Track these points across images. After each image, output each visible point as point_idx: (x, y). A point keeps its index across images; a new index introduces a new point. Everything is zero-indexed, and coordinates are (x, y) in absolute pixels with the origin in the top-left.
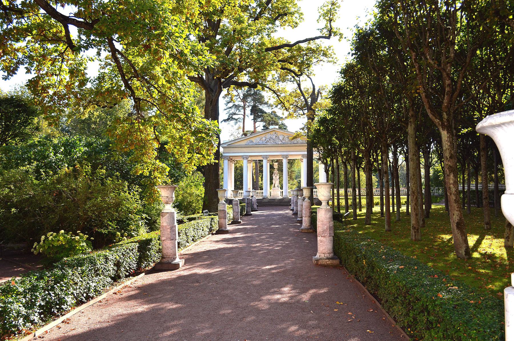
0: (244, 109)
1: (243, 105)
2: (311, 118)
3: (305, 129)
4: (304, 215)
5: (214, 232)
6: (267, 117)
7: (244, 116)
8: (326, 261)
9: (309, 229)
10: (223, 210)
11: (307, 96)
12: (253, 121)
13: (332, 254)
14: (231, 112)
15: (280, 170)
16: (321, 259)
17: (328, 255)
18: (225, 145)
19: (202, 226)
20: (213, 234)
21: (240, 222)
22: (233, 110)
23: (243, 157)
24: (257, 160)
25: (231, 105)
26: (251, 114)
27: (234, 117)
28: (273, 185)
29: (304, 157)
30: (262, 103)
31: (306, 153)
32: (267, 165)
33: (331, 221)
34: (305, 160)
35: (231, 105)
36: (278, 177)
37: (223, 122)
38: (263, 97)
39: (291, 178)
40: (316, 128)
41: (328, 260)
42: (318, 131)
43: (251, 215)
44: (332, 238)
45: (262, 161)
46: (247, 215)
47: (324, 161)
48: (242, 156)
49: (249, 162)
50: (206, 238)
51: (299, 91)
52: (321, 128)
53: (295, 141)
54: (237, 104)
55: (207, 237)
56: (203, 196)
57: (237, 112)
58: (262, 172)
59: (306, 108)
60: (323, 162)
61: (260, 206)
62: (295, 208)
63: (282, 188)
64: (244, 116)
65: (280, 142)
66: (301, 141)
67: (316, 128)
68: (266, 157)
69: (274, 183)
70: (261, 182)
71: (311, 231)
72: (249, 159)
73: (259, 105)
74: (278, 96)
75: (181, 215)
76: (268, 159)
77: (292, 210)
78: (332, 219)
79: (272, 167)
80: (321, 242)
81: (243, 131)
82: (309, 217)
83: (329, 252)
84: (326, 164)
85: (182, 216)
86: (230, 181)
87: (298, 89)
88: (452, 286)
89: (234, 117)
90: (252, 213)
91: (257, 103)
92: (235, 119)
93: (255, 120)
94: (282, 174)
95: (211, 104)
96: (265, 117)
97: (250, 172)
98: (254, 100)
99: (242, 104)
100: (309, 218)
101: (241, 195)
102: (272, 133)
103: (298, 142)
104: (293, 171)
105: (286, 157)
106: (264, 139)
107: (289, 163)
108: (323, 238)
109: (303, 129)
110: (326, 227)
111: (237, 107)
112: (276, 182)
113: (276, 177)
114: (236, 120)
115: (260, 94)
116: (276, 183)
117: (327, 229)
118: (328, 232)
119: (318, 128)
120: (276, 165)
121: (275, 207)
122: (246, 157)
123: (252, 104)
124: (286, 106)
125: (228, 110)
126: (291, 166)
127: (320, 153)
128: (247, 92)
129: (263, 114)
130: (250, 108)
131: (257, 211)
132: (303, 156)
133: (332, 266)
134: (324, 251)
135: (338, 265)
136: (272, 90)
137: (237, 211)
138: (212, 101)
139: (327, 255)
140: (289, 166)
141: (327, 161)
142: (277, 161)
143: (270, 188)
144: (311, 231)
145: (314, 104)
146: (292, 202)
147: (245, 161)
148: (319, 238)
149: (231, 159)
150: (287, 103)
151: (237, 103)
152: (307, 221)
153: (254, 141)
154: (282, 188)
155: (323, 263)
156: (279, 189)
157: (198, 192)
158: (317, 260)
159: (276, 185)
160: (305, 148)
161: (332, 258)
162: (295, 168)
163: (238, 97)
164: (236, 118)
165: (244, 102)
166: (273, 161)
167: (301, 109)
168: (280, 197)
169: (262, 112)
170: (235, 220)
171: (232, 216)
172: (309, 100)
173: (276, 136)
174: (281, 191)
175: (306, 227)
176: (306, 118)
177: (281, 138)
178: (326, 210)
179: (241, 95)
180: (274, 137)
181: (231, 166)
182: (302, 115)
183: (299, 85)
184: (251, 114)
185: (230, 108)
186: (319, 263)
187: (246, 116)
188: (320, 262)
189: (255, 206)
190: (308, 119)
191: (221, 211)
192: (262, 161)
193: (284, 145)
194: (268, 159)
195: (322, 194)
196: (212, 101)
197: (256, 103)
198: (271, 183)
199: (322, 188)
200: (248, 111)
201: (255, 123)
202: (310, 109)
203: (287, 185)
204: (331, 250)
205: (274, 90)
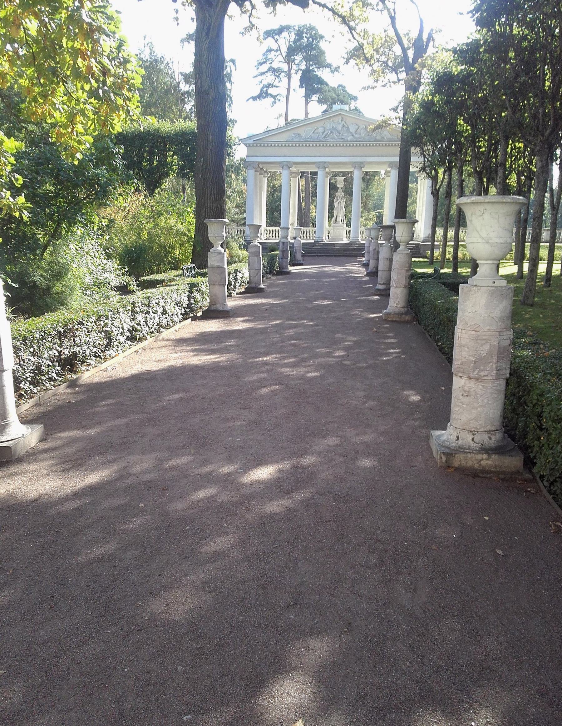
0: (289, 77)
1: (286, 69)
2: (413, 87)
3: (399, 110)
4: (393, 283)
5: (199, 314)
6: (329, 91)
7: (288, 90)
8: (479, 457)
9: (402, 314)
10: (219, 267)
11: (406, 43)
12: (304, 98)
13: (498, 436)
14: (265, 82)
15: (349, 192)
16: (460, 450)
17: (486, 437)
18: (250, 142)
19: (162, 303)
20: (195, 318)
21: (261, 290)
22: (269, 78)
23: (282, 165)
24: (308, 173)
25: (265, 68)
26: (301, 86)
27: (271, 91)
28: (334, 218)
29: (392, 167)
30: (322, 65)
31: (397, 159)
32: (324, 182)
33: (507, 329)
34: (394, 173)
35: (265, 68)
36: (343, 205)
37: (251, 100)
38: (324, 53)
39: (365, 207)
40: (426, 99)
41: (485, 456)
42: (427, 106)
43: (289, 273)
44: (503, 383)
45: (315, 174)
46: (283, 273)
47: (431, 173)
48: (280, 163)
49: (293, 175)
50: (172, 330)
51: (392, 33)
52: (436, 99)
53: (377, 135)
54: (276, 68)
55: (178, 326)
56: (193, 234)
57: (276, 83)
58: (314, 195)
59: (403, 69)
60: (429, 176)
61: (309, 256)
62: (372, 263)
63: (348, 225)
64: (288, 90)
65: (350, 138)
66: (389, 136)
67: (426, 99)
68: (323, 166)
69: (335, 215)
70: (314, 214)
71: (408, 318)
72: (294, 169)
73: (316, 70)
74: (351, 29)
75: (123, 274)
76: (327, 170)
77: (366, 265)
78: (509, 322)
79: (333, 188)
80: (467, 394)
81: (286, 119)
82: (405, 287)
83: (489, 428)
84: (434, 179)
85: (127, 278)
86: (258, 208)
87: (391, 26)
88: (548, 351)
89: (271, 91)
90: (290, 268)
91: (312, 65)
92: (271, 96)
93: (307, 97)
94: (351, 200)
95: (207, 34)
96: (325, 91)
97: (295, 194)
98: (307, 59)
99: (285, 67)
100: (405, 291)
101: (308, 235)
102: (336, 119)
103: (383, 138)
104: (370, 196)
105: (360, 165)
106: (321, 130)
107: (363, 179)
108: (473, 382)
109: (395, 110)
110: (487, 347)
111: (275, 71)
112: (340, 213)
113: (340, 204)
114: (274, 97)
115: (319, 48)
116: (339, 215)
117: (490, 354)
118: (492, 365)
119: (430, 97)
120: (340, 182)
121: (334, 258)
122: (288, 165)
123: (304, 67)
124: (366, 51)
125: (260, 78)
126: (367, 187)
127: (425, 157)
128: (295, 42)
129: (323, 86)
130: (300, 73)
131: (302, 265)
132: (391, 164)
133: (497, 473)
134: (473, 425)
135: (518, 472)
136: (340, 16)
137: (256, 266)
138: (208, 29)
139: (484, 439)
140: (363, 186)
141: (437, 172)
142: (344, 174)
143: (330, 225)
144: (408, 318)
145: (420, 60)
146: (366, 249)
147: (285, 173)
148: (458, 383)
149: (262, 169)
150: (367, 46)
151: (275, 65)
152: (399, 296)
153: (304, 135)
154: (348, 225)
155: (469, 464)
156: (345, 226)
157: (181, 228)
158: (450, 453)
159: (339, 219)
160: (397, 150)
161: (498, 450)
162: (374, 190)
163: (279, 52)
164: (274, 94)
165: (288, 64)
166: (335, 175)
167: (395, 70)
168: (345, 241)
169: (321, 81)
170: (253, 285)
171: (247, 275)
172: (411, 54)
173: (344, 126)
174: (348, 229)
175: (397, 310)
176: (403, 87)
177: (352, 129)
178: (495, 292)
179: (284, 49)
180: (340, 127)
181: (261, 182)
182: (394, 82)
183: (393, 19)
184: (301, 86)
185: (264, 73)
186: (456, 464)
187: (291, 90)
188: (459, 460)
189: (299, 257)
190: (407, 89)
191: (213, 268)
192: (315, 174)
193: (358, 143)
194: (327, 170)
195: (484, 234)
196: (208, 29)
197: (310, 65)
198: (331, 216)
199: (486, 216)
200: (296, 79)
201: (307, 103)
202: (410, 68)
203: (359, 219)
204: (497, 422)
205: (344, 14)
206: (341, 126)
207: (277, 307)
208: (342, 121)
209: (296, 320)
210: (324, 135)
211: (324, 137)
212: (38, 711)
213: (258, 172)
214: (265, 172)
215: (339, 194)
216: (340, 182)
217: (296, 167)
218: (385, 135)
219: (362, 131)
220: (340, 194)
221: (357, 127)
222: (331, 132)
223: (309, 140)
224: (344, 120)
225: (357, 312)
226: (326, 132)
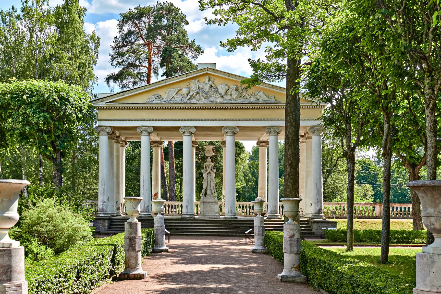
69: (204, 187)
102: (202, 80)
103: (258, 99)
149: (118, 137)
173: (211, 86)
206: (208, 86)
207: (363, 274)
208: (209, 81)
209: (190, 284)
210: (189, 97)
211: (189, 99)
212: (335, 147)
213: (113, 139)
214: (123, 141)
215: (208, 164)
216: (209, 152)
217: (158, 135)
218: (260, 97)
219: (234, 92)
220: (209, 163)
221: (227, 88)
222: (198, 93)
223: (172, 102)
224: (212, 79)
225: (169, 250)
226: (191, 93)
